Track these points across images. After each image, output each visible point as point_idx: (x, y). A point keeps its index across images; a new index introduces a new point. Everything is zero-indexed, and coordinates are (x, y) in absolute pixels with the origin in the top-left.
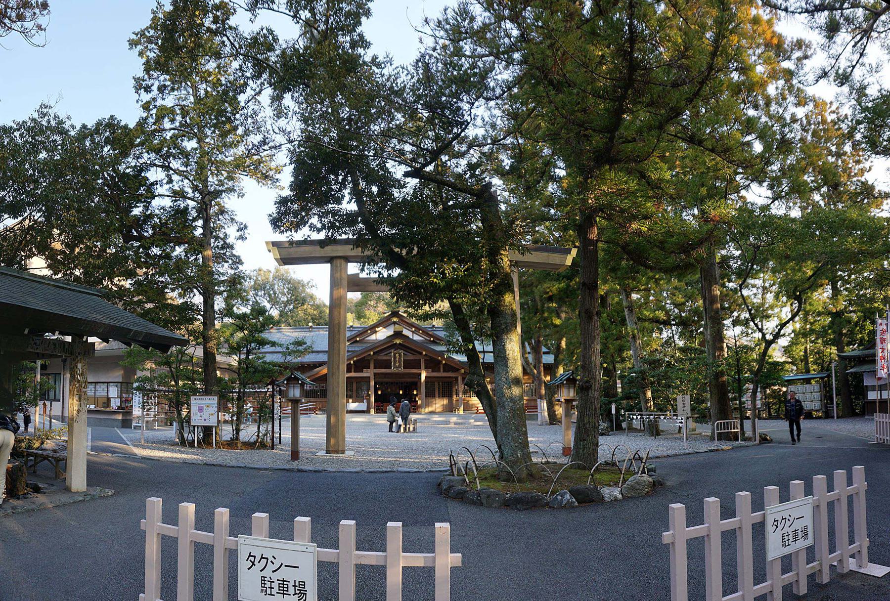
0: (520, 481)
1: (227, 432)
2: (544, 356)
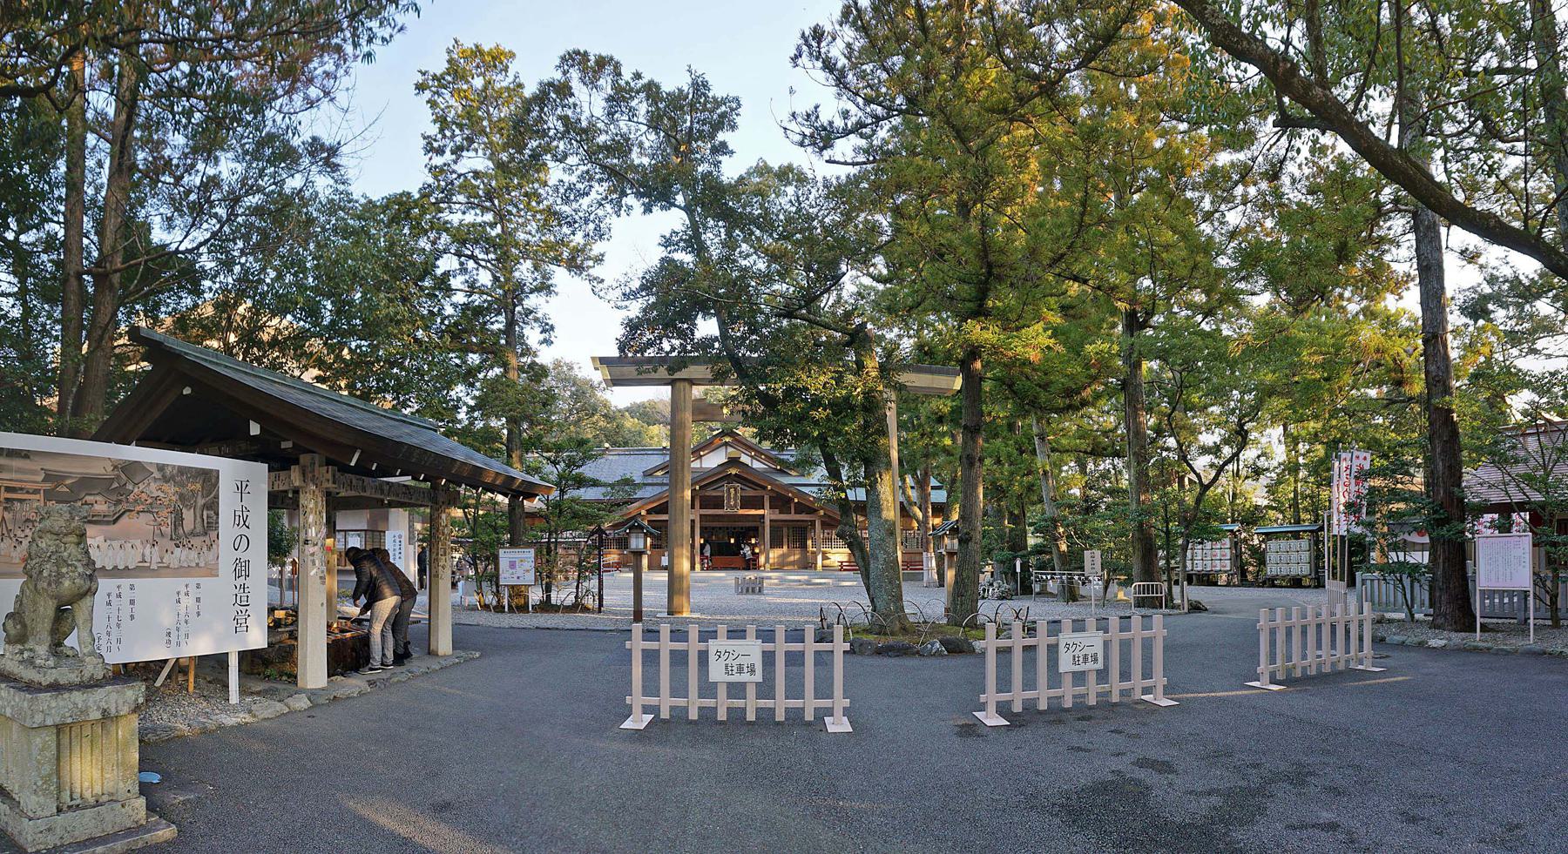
0: (893, 634)
1: (536, 596)
2: (933, 493)
